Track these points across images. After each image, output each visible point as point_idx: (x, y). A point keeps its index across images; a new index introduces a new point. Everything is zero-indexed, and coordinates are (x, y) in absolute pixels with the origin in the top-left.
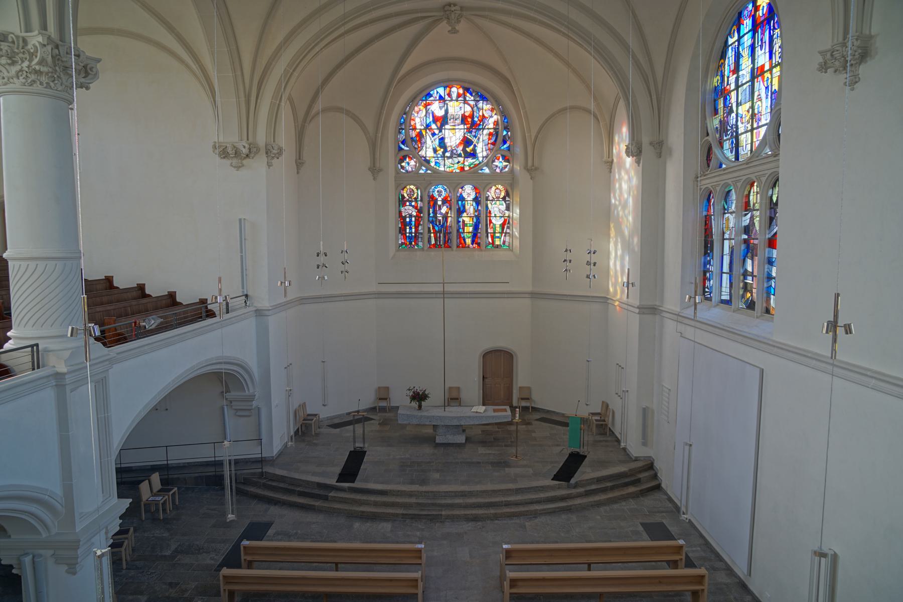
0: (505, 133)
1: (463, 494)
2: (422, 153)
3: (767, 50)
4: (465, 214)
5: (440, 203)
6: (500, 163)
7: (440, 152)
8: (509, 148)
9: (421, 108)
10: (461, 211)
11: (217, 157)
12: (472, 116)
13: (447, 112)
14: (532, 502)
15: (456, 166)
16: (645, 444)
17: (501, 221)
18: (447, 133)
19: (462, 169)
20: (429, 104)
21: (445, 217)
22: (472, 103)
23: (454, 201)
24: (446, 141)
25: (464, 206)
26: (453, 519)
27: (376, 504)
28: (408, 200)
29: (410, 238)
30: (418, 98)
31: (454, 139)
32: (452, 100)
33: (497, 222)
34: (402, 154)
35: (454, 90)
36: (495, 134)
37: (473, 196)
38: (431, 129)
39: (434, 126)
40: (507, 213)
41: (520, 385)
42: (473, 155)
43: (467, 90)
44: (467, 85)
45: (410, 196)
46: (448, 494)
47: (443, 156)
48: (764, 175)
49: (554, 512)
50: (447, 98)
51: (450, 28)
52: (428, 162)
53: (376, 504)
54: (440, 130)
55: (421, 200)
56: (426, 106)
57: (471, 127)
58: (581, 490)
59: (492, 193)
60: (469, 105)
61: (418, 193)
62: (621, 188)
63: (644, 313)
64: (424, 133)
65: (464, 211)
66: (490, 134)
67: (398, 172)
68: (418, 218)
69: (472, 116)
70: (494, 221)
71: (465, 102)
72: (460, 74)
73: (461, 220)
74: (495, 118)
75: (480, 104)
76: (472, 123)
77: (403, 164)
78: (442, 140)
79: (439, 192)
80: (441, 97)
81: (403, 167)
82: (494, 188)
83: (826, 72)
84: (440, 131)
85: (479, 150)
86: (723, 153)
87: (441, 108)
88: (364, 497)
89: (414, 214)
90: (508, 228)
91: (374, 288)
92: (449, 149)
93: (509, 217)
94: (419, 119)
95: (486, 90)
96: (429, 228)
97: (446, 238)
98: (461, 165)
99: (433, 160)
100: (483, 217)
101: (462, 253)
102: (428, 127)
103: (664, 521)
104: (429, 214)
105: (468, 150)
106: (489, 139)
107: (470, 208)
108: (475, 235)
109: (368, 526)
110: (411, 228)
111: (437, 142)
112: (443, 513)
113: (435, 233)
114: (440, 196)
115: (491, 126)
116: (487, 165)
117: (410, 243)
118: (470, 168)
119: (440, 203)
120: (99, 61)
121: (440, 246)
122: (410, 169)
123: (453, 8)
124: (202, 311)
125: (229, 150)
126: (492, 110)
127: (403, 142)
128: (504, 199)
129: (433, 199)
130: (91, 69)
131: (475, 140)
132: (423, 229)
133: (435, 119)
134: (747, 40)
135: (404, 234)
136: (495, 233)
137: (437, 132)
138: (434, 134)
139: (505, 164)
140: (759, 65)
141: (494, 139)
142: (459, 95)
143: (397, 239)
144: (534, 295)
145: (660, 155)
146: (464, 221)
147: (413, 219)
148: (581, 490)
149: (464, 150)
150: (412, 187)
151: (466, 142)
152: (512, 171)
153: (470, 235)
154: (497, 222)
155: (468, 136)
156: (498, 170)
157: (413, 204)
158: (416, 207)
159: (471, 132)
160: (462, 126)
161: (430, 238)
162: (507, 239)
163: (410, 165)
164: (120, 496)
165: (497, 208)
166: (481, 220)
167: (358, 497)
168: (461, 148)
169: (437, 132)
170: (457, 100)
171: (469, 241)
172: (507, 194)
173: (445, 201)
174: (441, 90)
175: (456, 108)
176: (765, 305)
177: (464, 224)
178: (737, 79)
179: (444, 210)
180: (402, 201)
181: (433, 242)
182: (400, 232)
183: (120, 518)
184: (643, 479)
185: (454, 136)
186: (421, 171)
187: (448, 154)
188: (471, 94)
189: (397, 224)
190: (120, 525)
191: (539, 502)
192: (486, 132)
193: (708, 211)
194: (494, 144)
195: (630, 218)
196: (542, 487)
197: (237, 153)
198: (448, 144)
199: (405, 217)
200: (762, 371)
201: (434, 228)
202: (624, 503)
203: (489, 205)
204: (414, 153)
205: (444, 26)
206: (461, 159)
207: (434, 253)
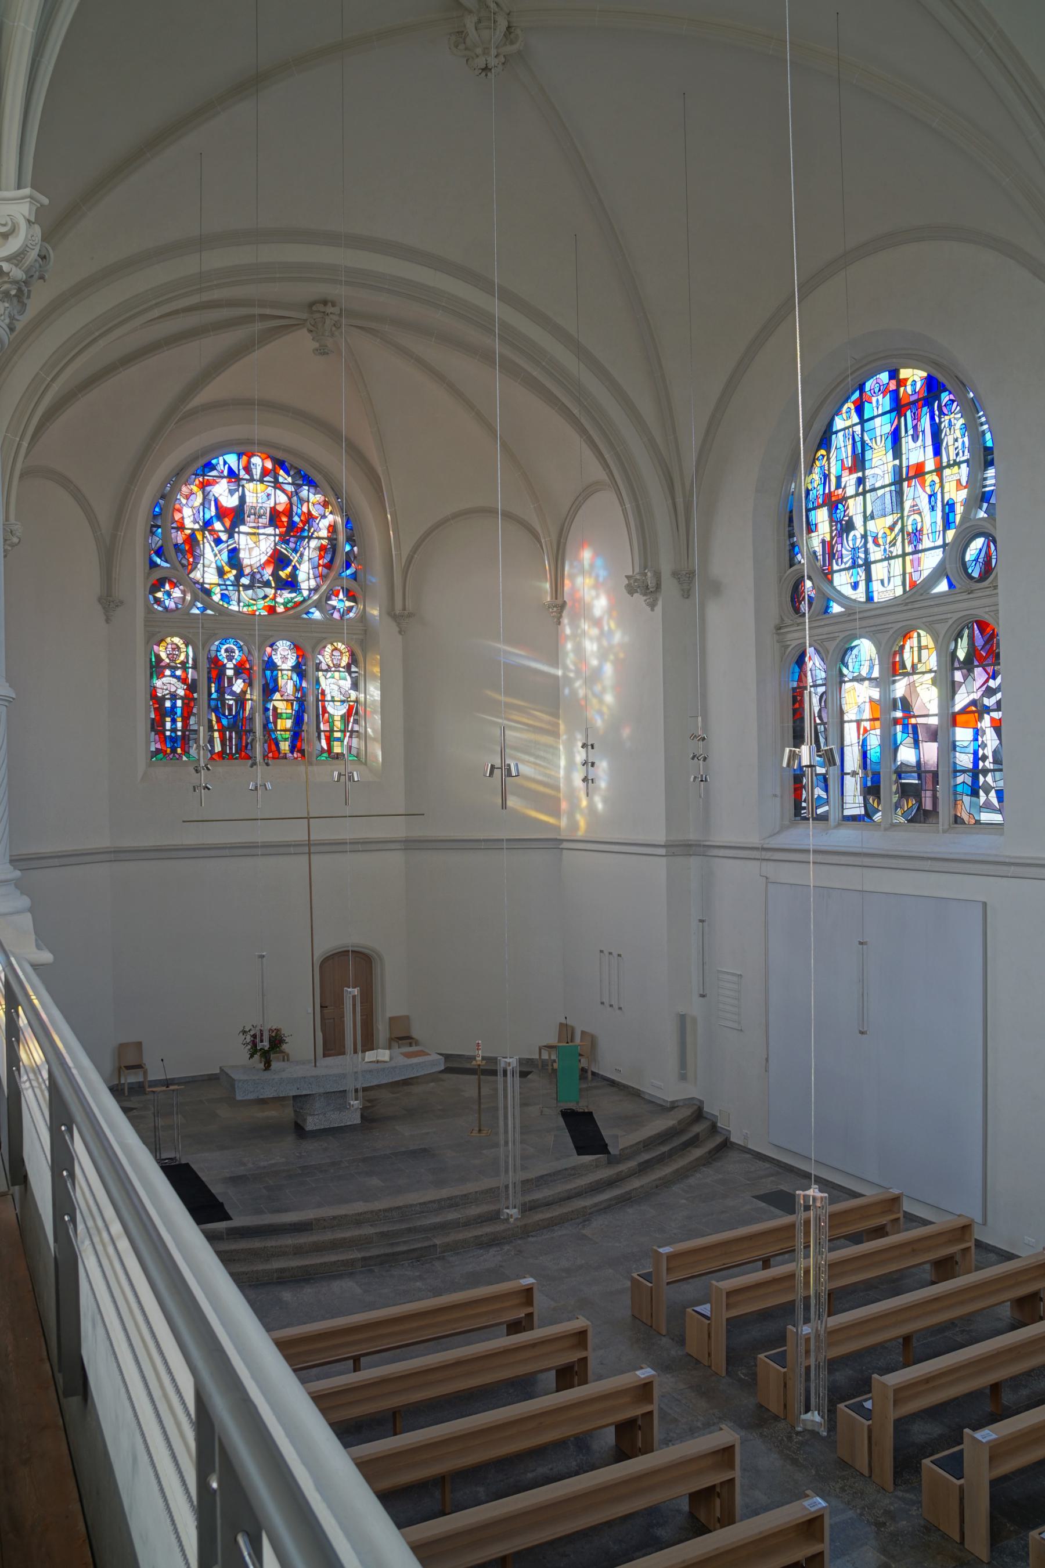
0: (348, 548)
1: (453, 1203)
2: (196, 575)
3: (929, 441)
4: (277, 696)
5: (230, 673)
6: (339, 602)
7: (231, 575)
8: (354, 576)
9: (195, 489)
10: (270, 689)
11: (625, 591)
12: (289, 512)
13: (242, 499)
14: (570, 1197)
15: (261, 603)
16: (683, 1077)
17: (343, 710)
18: (243, 541)
19: (272, 610)
20: (209, 483)
21: (241, 699)
22: (290, 488)
23: (257, 669)
24: (242, 555)
25: (276, 681)
26: (456, 1248)
27: (299, 1251)
28: (168, 666)
29: (173, 740)
30: (192, 469)
31: (256, 552)
32: (252, 480)
33: (337, 711)
34: (157, 575)
35: (256, 460)
36: (329, 549)
37: (291, 662)
38: (212, 532)
39: (218, 526)
40: (353, 695)
41: (389, 1014)
42: (292, 584)
43: (280, 464)
44: (280, 455)
45: (172, 657)
46: (426, 1208)
47: (236, 583)
48: (946, 620)
49: (609, 1207)
50: (242, 474)
51: (316, 345)
52: (208, 593)
53: (299, 1251)
54: (230, 532)
55: (195, 667)
56: (203, 486)
57: (287, 533)
58: (632, 1164)
59: (326, 658)
60: (284, 491)
61: (187, 653)
62: (579, 650)
63: (674, 855)
64: (199, 537)
65: (276, 689)
66: (322, 548)
67: (149, 610)
68: (188, 700)
69: (289, 512)
70: (330, 709)
71: (277, 485)
72: (258, 431)
74: (330, 518)
75: (304, 492)
76: (290, 527)
77: (159, 595)
78: (234, 552)
79: (229, 653)
80: (230, 470)
81: (158, 601)
82: (329, 648)
84: (231, 536)
85: (301, 576)
86: (834, 588)
87: (232, 492)
88: (271, 1243)
89: (181, 693)
90: (356, 722)
91: (103, 841)
92: (247, 571)
93: (357, 701)
94: (189, 513)
95: (314, 466)
96: (210, 721)
97: (241, 737)
99: (217, 590)
100: (311, 699)
101: (277, 769)
102: (207, 524)
103: (782, 1187)
104: (210, 694)
105: (283, 574)
106: (320, 557)
107: (287, 683)
108: (296, 735)
109: (308, 1292)
110: (174, 721)
111: (225, 555)
112: (437, 1242)
113: (222, 731)
114: (230, 658)
115: (324, 533)
116: (317, 605)
117: (174, 750)
118: (287, 609)
119: (230, 673)
121: (231, 756)
122: (173, 605)
123: (329, 309)
126: (325, 505)
127: (159, 552)
128: (348, 668)
129: (216, 667)
131: (295, 558)
132: (198, 723)
133: (222, 513)
134: (882, 426)
135: (161, 733)
136: (332, 731)
137: (224, 537)
138: (218, 541)
139: (348, 604)
140: (913, 461)
141: (328, 557)
142: (265, 472)
143: (148, 744)
144: (410, 844)
145: (687, 594)
146: (275, 709)
147: (179, 703)
148: (632, 1164)
149: (275, 574)
150: (176, 640)
151: (279, 560)
152: (363, 617)
153: (287, 735)
154: (337, 711)
155: (282, 548)
156: (336, 615)
157: (179, 673)
158: (184, 681)
159: (287, 542)
160: (270, 530)
161: (211, 741)
162: (355, 742)
163: (173, 596)
165: (334, 685)
166: (307, 707)
167: (256, 1244)
169: (224, 537)
170: (261, 481)
171: (285, 746)
172: (354, 660)
173: (239, 670)
174: (232, 459)
175: (260, 496)
176: (952, 813)
177: (277, 715)
178: (861, 481)
179: (238, 686)
180: (157, 668)
181: (218, 748)
182: (153, 729)
184: (696, 1136)
185: (256, 548)
186: (195, 611)
187: (245, 581)
188: (287, 473)
189: (148, 712)
191: (579, 1194)
192: (314, 543)
193: (800, 679)
194: (329, 566)
195: (609, 698)
196: (574, 1168)
198: (246, 562)
199: (164, 698)
200: (985, 904)
201: (219, 721)
202: (698, 1175)
203: (322, 680)
204: (181, 576)
206: (270, 592)
207: (222, 768)
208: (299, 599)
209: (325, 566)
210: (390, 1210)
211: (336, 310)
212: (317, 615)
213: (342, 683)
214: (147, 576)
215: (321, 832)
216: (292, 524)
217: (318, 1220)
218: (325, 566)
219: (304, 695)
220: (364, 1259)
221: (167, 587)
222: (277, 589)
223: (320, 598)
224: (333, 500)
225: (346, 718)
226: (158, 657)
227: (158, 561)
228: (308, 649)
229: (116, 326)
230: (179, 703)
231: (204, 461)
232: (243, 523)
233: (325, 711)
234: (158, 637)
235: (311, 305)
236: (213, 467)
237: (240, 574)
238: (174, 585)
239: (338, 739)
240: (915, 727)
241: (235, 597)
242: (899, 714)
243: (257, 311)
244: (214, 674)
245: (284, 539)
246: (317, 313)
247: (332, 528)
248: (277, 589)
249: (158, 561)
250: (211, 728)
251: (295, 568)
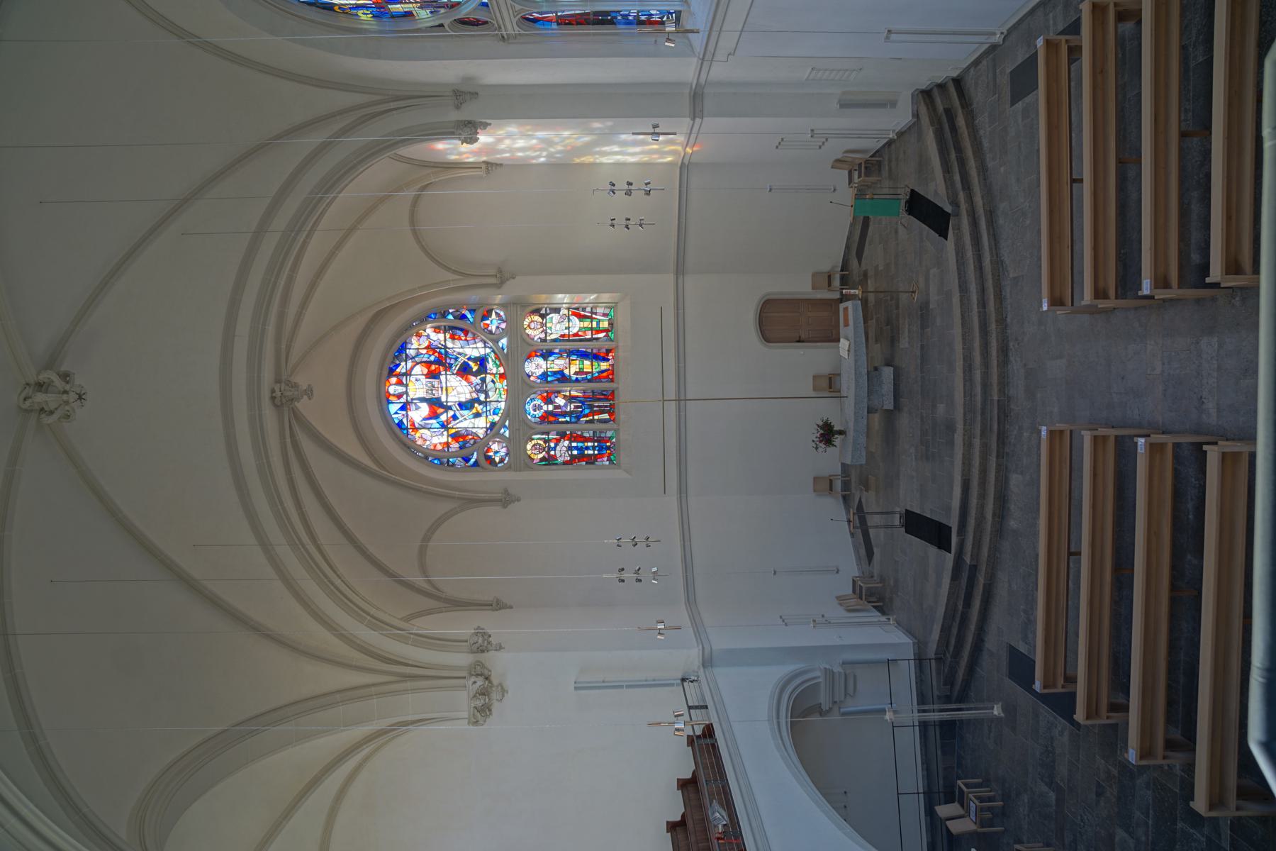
1: (968, 369)
2: (481, 433)
4: (566, 372)
5: (551, 407)
6: (493, 323)
7: (479, 407)
8: (472, 311)
9: (418, 435)
10: (562, 377)
12: (428, 364)
13: (422, 400)
14: (980, 268)
15: (498, 385)
16: (893, 104)
17: (575, 319)
18: (453, 399)
19: (502, 376)
20: (413, 424)
21: (571, 399)
22: (410, 364)
24: (463, 400)
25: (555, 373)
26: (1004, 383)
27: (982, 496)
28: (548, 453)
29: (601, 449)
30: (405, 439)
31: (460, 389)
32: (406, 393)
33: (576, 325)
34: (483, 461)
35: (392, 390)
36: (453, 331)
37: (540, 361)
38: (448, 422)
39: (443, 418)
40: (564, 312)
42: (482, 361)
43: (391, 372)
44: (386, 372)
45: (542, 450)
46: (968, 393)
47: (485, 403)
50: (403, 400)
52: (493, 425)
53: (982, 496)
54: (448, 408)
55: (548, 434)
56: (415, 429)
57: (444, 365)
58: (962, 196)
59: (536, 334)
60: (412, 368)
61: (538, 439)
62: (522, 149)
63: (702, 111)
64: (452, 431)
66: (452, 337)
68: (573, 438)
69: (428, 364)
70: (574, 331)
71: (408, 374)
73: (574, 377)
74: (429, 331)
75: (411, 352)
76: (438, 363)
77: (497, 460)
79: (534, 408)
81: (502, 460)
82: (528, 331)
84: (450, 408)
85: (475, 354)
88: (973, 512)
89: (566, 443)
90: (584, 309)
92: (475, 395)
93: (569, 309)
94: (433, 439)
97: (600, 397)
99: (490, 418)
100: (569, 346)
102: (444, 426)
103: (1008, 71)
104: (567, 422)
105: (475, 368)
107: (557, 364)
108: (596, 357)
110: (587, 448)
111: (465, 412)
112: (996, 398)
113: (594, 413)
115: (441, 336)
116: (496, 341)
117: (608, 448)
118: (501, 365)
119: (551, 407)
121: (612, 406)
122: (504, 450)
123: (278, 394)
124: (704, 743)
125: (479, 703)
126: (419, 336)
127: (467, 460)
128: (543, 316)
131: (462, 359)
132: (588, 430)
133: (433, 415)
135: (596, 457)
136: (592, 329)
137: (451, 413)
139: (494, 316)
141: (459, 332)
142: (400, 383)
143: (603, 467)
146: (576, 373)
147: (574, 444)
149: (476, 374)
150: (529, 447)
151: (464, 371)
152: (503, 306)
153: (595, 364)
154: (576, 325)
155: (456, 369)
156: (503, 326)
157: (552, 445)
158: (558, 441)
159: (451, 365)
160: (443, 378)
161: (600, 421)
162: (600, 310)
163: (498, 450)
165: (557, 326)
168: (472, 378)
169: (451, 413)
170: (407, 386)
171: (604, 366)
172: (536, 312)
173: (548, 400)
174: (393, 408)
175: (418, 386)
177: (581, 372)
179: (560, 401)
180: (549, 461)
181: (606, 416)
184: (946, 104)
185: (457, 389)
186: (507, 434)
187: (482, 397)
188: (398, 366)
192: (449, 344)
193: (551, 21)
197: (484, 692)
198: (468, 397)
199: (571, 456)
202: (981, 132)
203: (553, 337)
204: (482, 444)
206: (489, 378)
207: (621, 415)
208: (493, 355)
209: (466, 335)
210: (965, 421)
211: (277, 388)
212: (504, 342)
213: (555, 321)
214: (485, 469)
215: (671, 393)
216: (439, 362)
217: (963, 475)
218: (466, 335)
219: (565, 351)
220: (998, 457)
221: (491, 454)
222: (486, 373)
223: (492, 340)
224: (414, 331)
225: (581, 317)
226: (542, 460)
227: (473, 460)
228: (529, 349)
229: (326, 576)
230: (574, 444)
231: (397, 429)
232: (439, 399)
233: (576, 335)
234: (527, 460)
235: (276, 406)
236: (401, 422)
237: (477, 401)
238: (489, 449)
239: (598, 324)
241: (494, 405)
243: (288, 440)
244: (552, 419)
245: (448, 367)
246: (285, 400)
247: (437, 330)
248: (486, 373)
249: (473, 460)
250: (591, 422)
251: (469, 359)
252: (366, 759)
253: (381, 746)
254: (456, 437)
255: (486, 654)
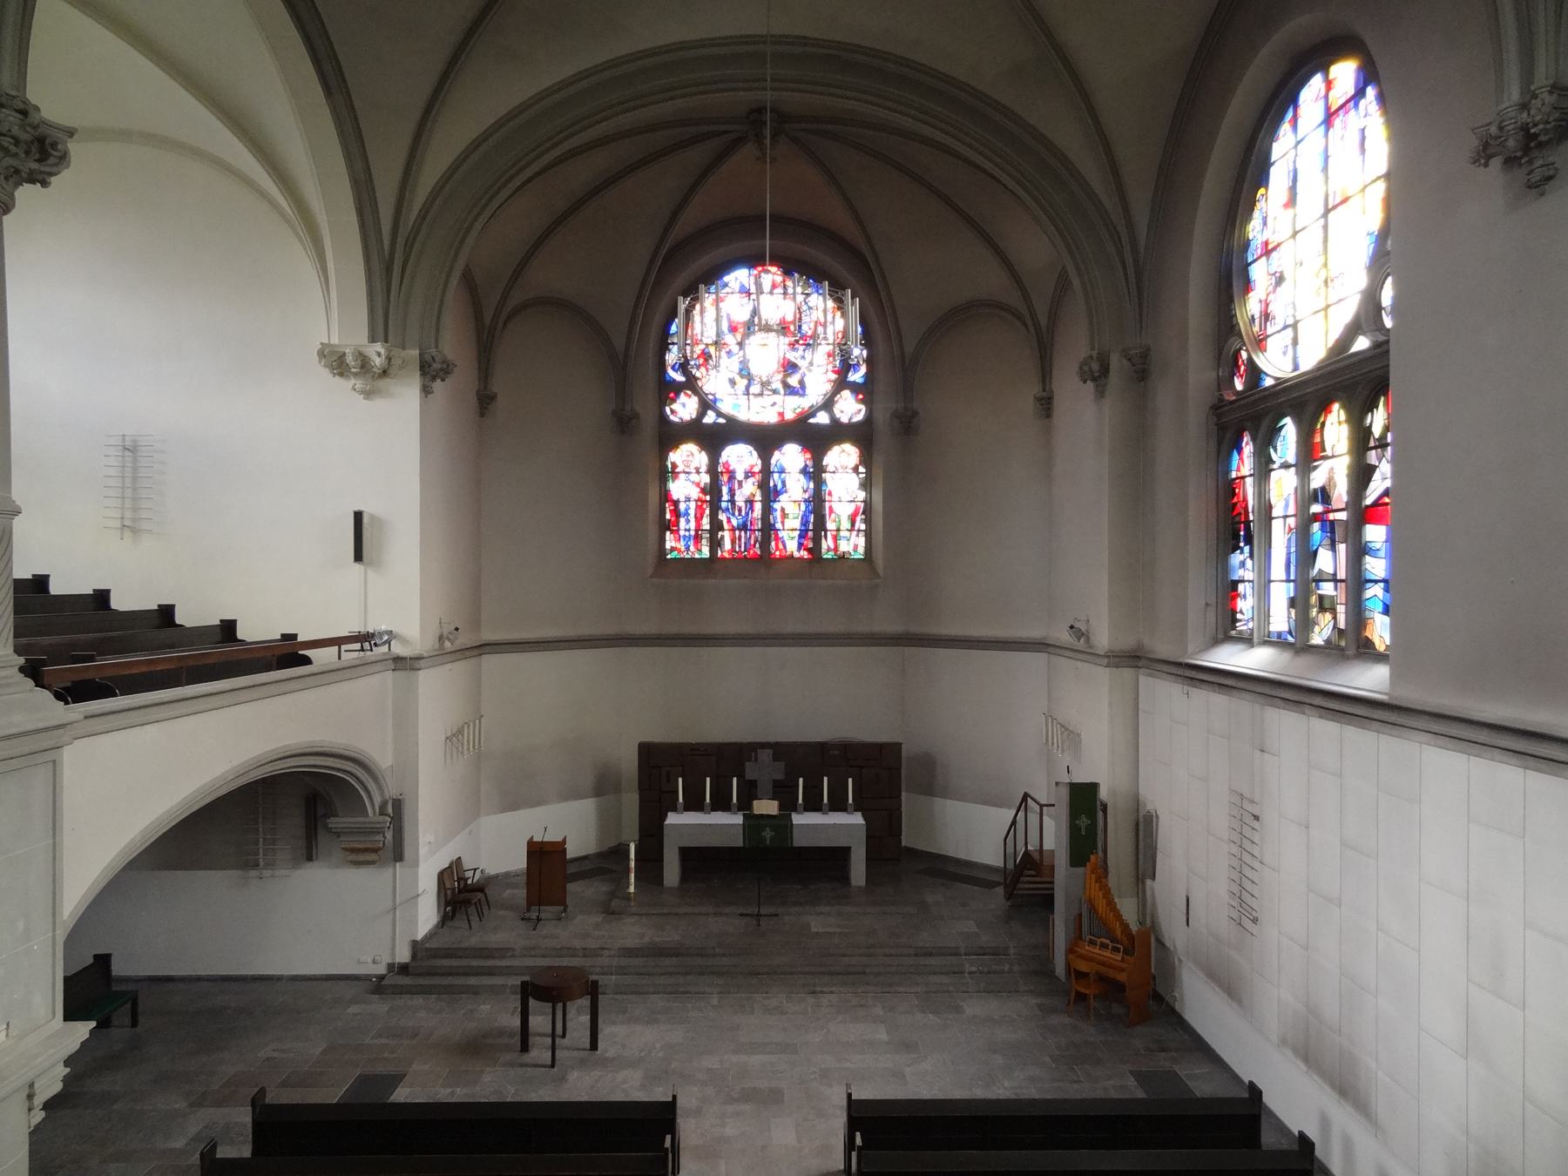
11: (326, 372)
73: (777, 506)
80: (742, 286)
83: (1486, 165)
98: (778, 409)
110: (688, 521)
120: (71, 133)
124: (287, 654)
125: (350, 359)
130: (54, 145)
137: (735, 349)
142: (774, 286)
151: (789, 367)
155: (792, 356)
164: (69, 1016)
168: (780, 376)
170: (771, 293)
175: (776, 307)
183: (67, 1063)
185: (766, 354)
187: (755, 389)
190: (67, 1080)
197: (364, 363)
201: (729, 521)
205: (749, 150)
240: (1332, 522)
242: (1317, 508)
245: (792, 345)
252: (282, 214)
253: (287, 221)
254: (747, 477)
255: (418, 373)
